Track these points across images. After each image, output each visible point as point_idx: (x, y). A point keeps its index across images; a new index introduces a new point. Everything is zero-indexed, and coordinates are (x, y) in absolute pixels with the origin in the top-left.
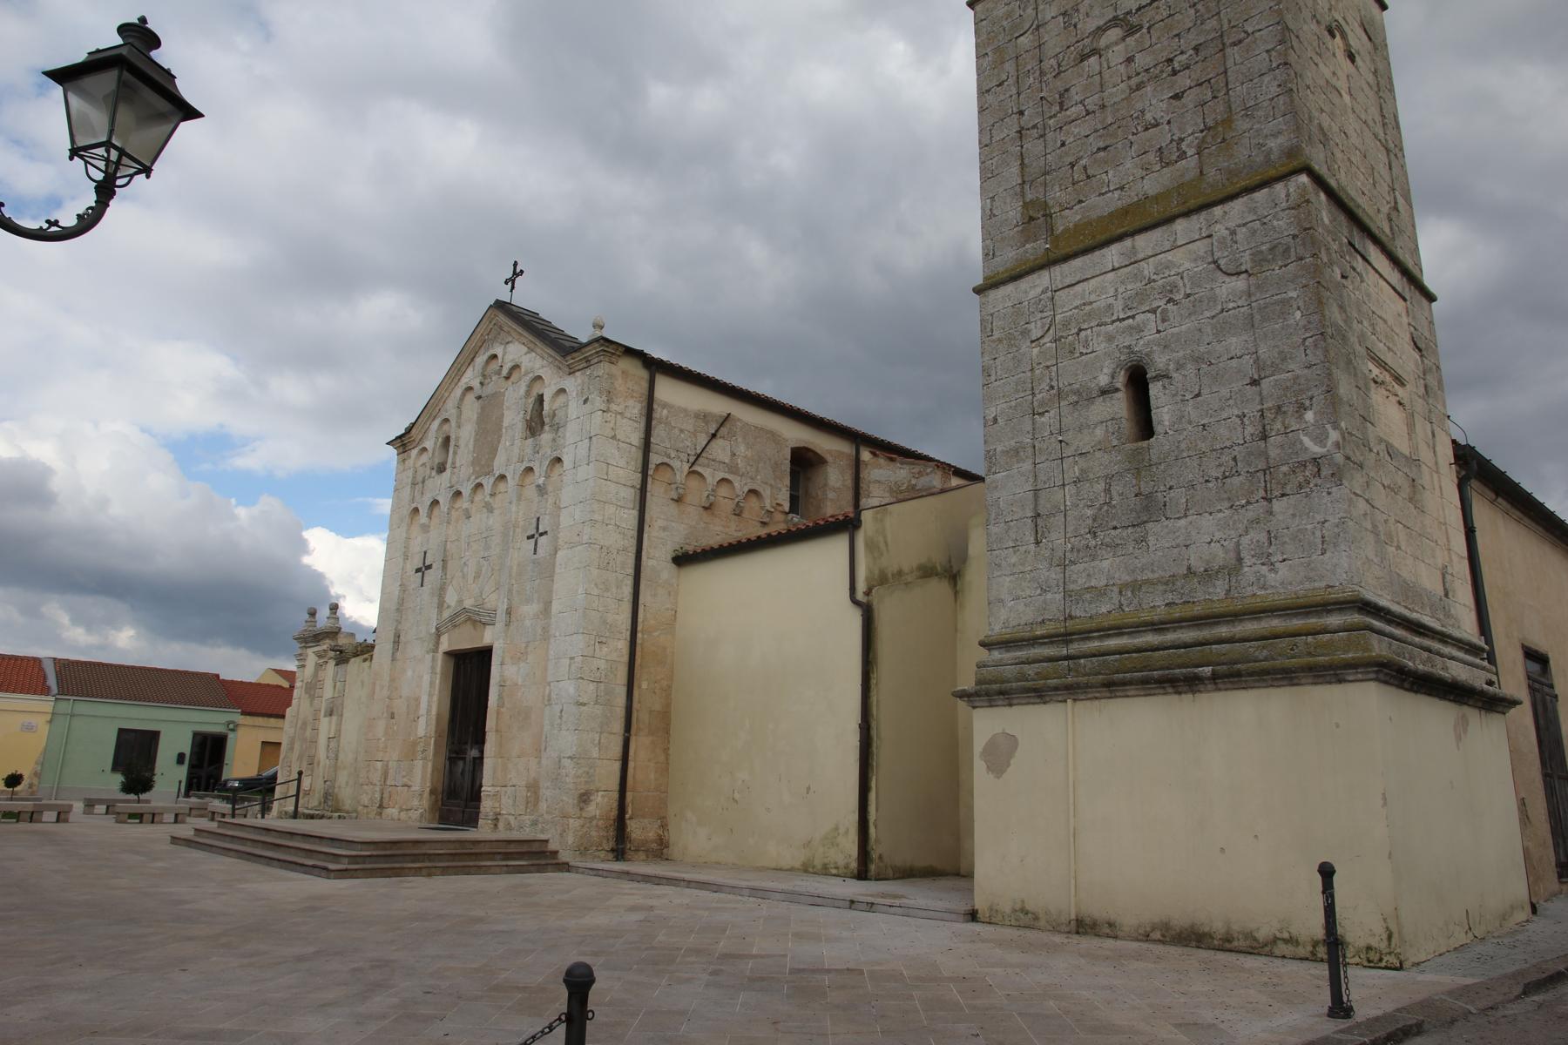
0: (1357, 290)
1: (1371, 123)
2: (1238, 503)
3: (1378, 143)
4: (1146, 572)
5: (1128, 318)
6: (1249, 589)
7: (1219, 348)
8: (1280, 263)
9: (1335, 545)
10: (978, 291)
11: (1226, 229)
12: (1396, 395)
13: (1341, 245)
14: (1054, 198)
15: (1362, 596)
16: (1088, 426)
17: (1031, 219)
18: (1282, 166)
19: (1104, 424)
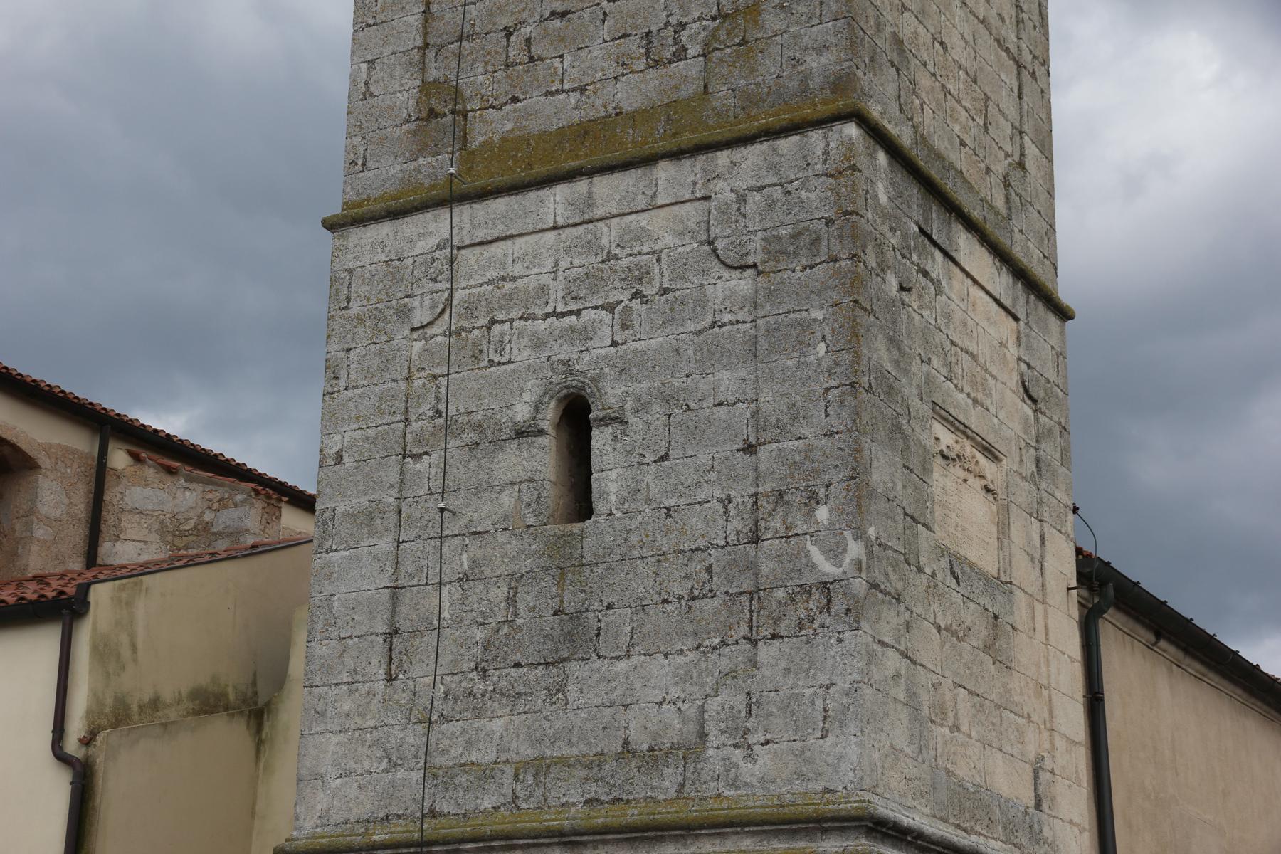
0: (928, 308)
1: (994, 21)
2: (707, 642)
3: (1004, 54)
4: (558, 744)
5: (571, 313)
6: (712, 784)
7: (703, 384)
8: (804, 261)
9: (842, 724)
10: (332, 225)
11: (732, 191)
12: (983, 477)
13: (905, 237)
14: (472, 84)
15: (871, 810)
16: (491, 488)
17: (433, 114)
18: (824, 103)
19: (516, 487)
